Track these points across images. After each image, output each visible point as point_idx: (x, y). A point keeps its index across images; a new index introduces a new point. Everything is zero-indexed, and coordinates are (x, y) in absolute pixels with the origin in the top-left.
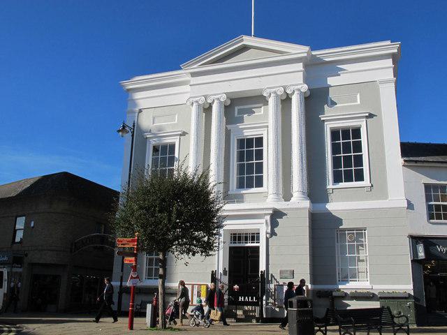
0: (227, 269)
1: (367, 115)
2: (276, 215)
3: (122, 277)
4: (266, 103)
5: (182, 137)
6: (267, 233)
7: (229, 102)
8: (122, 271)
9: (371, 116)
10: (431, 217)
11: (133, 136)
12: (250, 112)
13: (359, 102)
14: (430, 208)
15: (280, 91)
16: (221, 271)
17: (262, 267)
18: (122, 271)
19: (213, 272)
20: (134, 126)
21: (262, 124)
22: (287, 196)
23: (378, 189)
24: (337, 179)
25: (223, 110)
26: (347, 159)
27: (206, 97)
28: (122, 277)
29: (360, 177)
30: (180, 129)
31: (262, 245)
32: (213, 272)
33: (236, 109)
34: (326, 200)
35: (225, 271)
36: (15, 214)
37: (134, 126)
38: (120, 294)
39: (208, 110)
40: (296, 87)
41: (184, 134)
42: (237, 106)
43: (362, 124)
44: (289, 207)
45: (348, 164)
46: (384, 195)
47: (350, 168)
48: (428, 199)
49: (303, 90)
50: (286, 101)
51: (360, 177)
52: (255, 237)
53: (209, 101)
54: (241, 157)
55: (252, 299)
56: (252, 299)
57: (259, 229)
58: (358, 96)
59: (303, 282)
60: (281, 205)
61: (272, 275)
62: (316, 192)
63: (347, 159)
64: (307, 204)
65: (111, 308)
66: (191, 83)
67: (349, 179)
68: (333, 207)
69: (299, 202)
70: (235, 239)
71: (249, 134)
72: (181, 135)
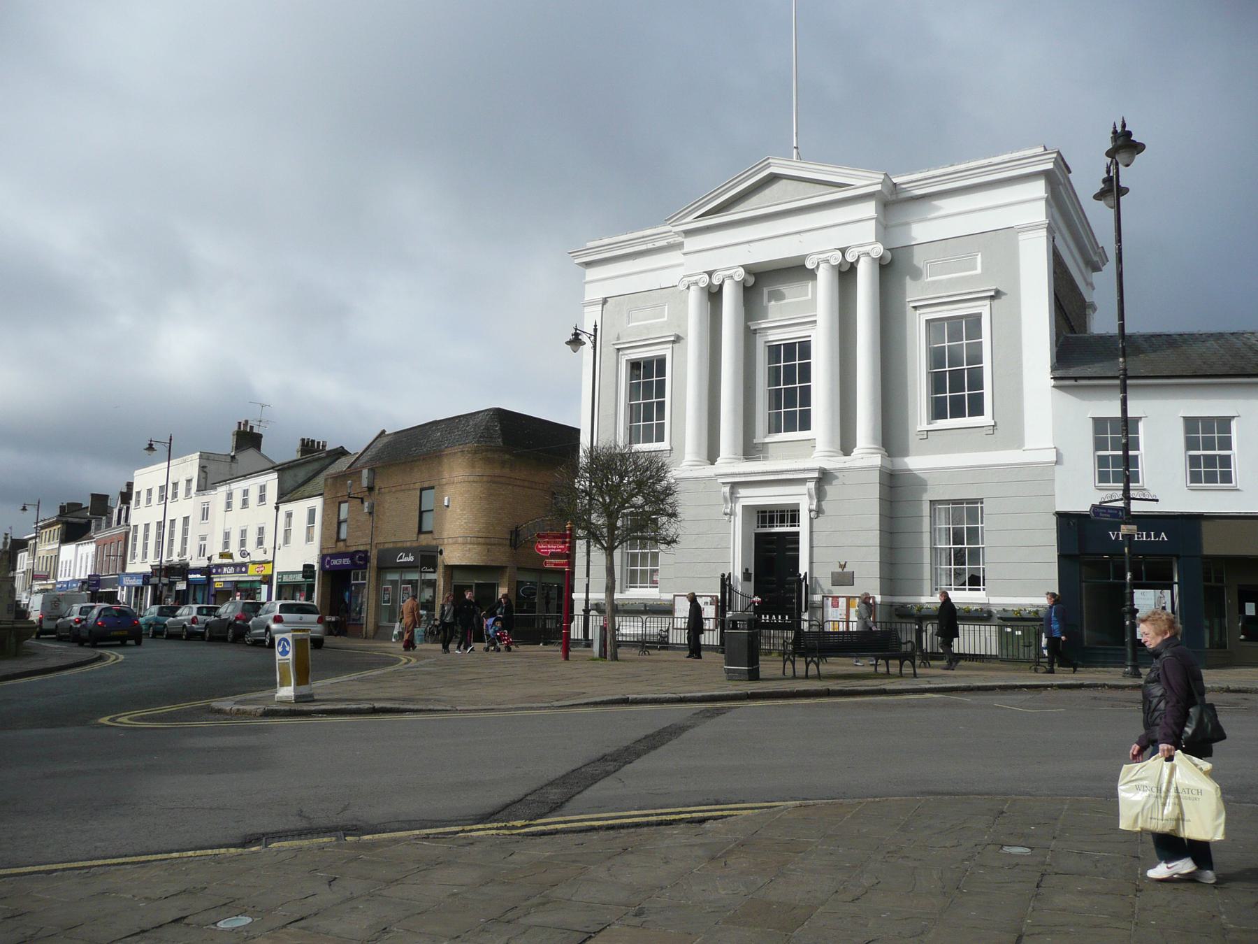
0: (752, 571)
1: (992, 293)
2: (824, 477)
3: (588, 586)
4: (811, 274)
5: (676, 345)
6: (810, 511)
7: (751, 281)
8: (588, 575)
9: (997, 295)
10: (1195, 478)
11: (595, 347)
12: (778, 296)
13: (979, 271)
14: (1194, 461)
15: (836, 258)
16: (738, 573)
17: (803, 568)
18: (588, 575)
19: (723, 575)
20: (595, 330)
21: (806, 315)
22: (847, 446)
23: (1009, 431)
24: (938, 411)
25: (706, 297)
26: (791, 393)
27: (843, 251)
28: (588, 586)
29: (977, 409)
30: (670, 333)
31: (803, 529)
32: (723, 575)
33: (766, 291)
34: (905, 452)
35: (746, 575)
36: (418, 486)
37: (595, 330)
38: (587, 611)
39: (714, 295)
40: (823, 256)
41: (677, 339)
42: (762, 282)
43: (984, 309)
44: (847, 465)
45: (790, 370)
46: (1017, 441)
47: (958, 391)
48: (1191, 444)
49: (875, 255)
50: (846, 274)
51: (977, 409)
52: (791, 515)
53: (850, 259)
54: (774, 376)
55: (783, 618)
56: (783, 618)
57: (982, 414)
58: (979, 258)
59: (725, 582)
60: (836, 463)
61: (749, 580)
62: (891, 436)
63: (791, 393)
64: (877, 460)
65: (1200, 679)
66: (685, 250)
67: (958, 412)
68: (914, 462)
69: (866, 454)
70: (764, 521)
71: (778, 337)
72: (674, 342)
